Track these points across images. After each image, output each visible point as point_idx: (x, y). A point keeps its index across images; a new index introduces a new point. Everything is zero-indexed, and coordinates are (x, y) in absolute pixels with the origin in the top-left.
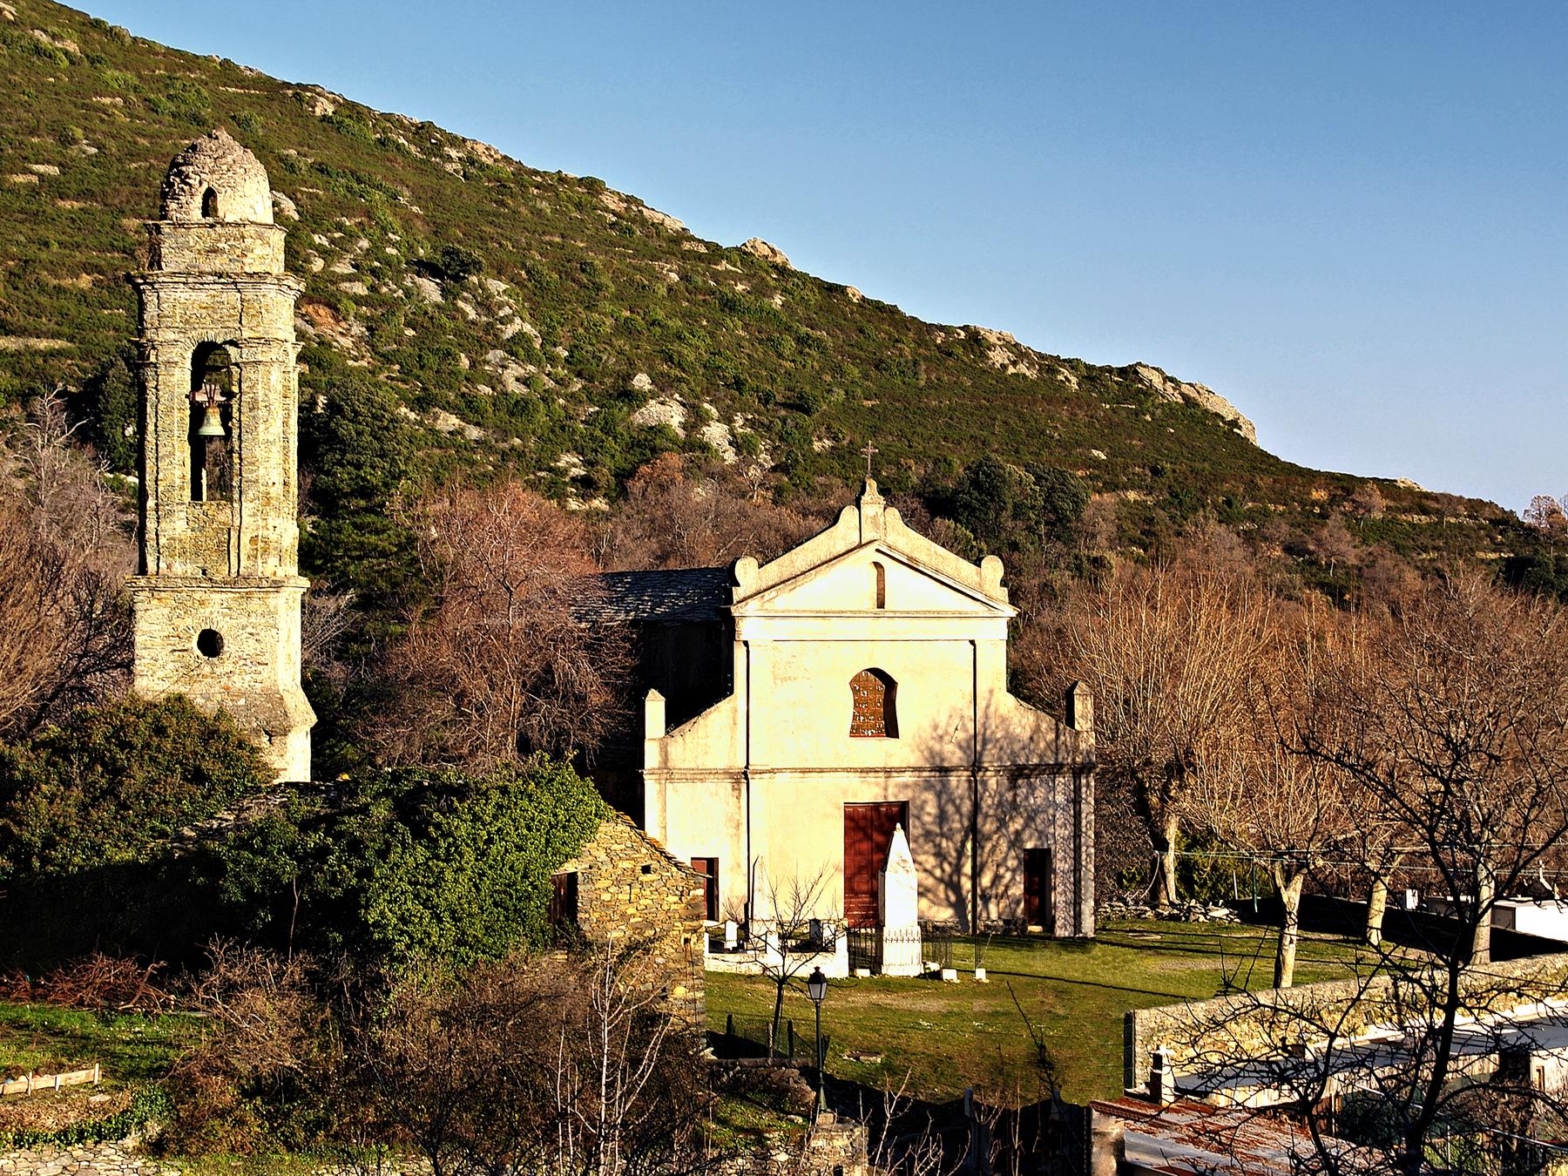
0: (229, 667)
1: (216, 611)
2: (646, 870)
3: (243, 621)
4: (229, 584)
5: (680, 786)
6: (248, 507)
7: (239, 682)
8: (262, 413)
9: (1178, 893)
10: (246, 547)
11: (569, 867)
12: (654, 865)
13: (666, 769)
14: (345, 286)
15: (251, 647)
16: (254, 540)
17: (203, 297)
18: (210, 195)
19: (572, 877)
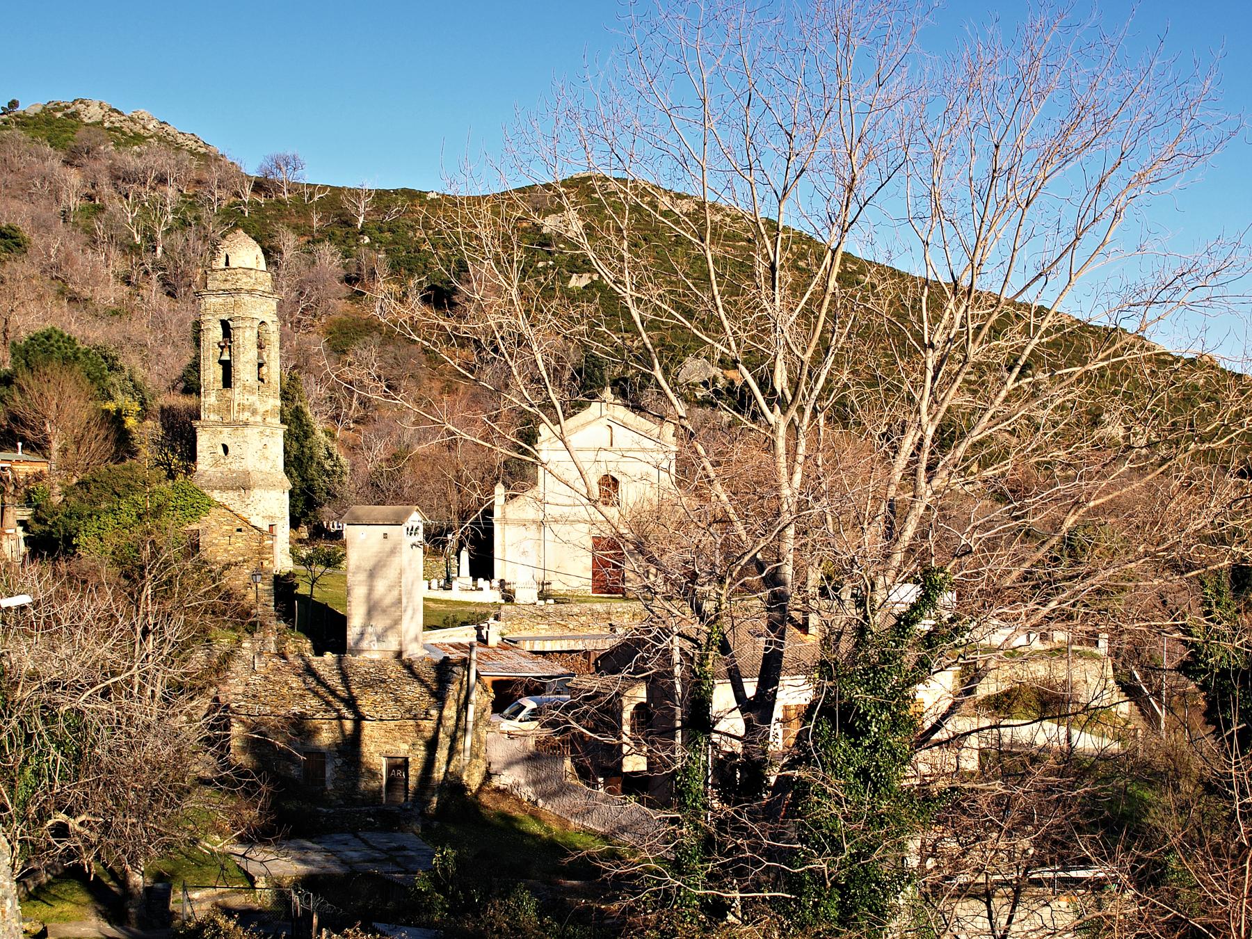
0: (230, 460)
1: (226, 436)
2: (239, 530)
3: (236, 440)
4: (228, 425)
5: (511, 526)
6: (237, 391)
7: (234, 467)
8: (241, 349)
9: (318, 843)
10: (236, 408)
11: (194, 527)
12: (244, 528)
13: (504, 520)
14: (1010, 631)
15: (238, 451)
16: (239, 405)
17: (220, 300)
18: (227, 257)
19: (197, 533)
